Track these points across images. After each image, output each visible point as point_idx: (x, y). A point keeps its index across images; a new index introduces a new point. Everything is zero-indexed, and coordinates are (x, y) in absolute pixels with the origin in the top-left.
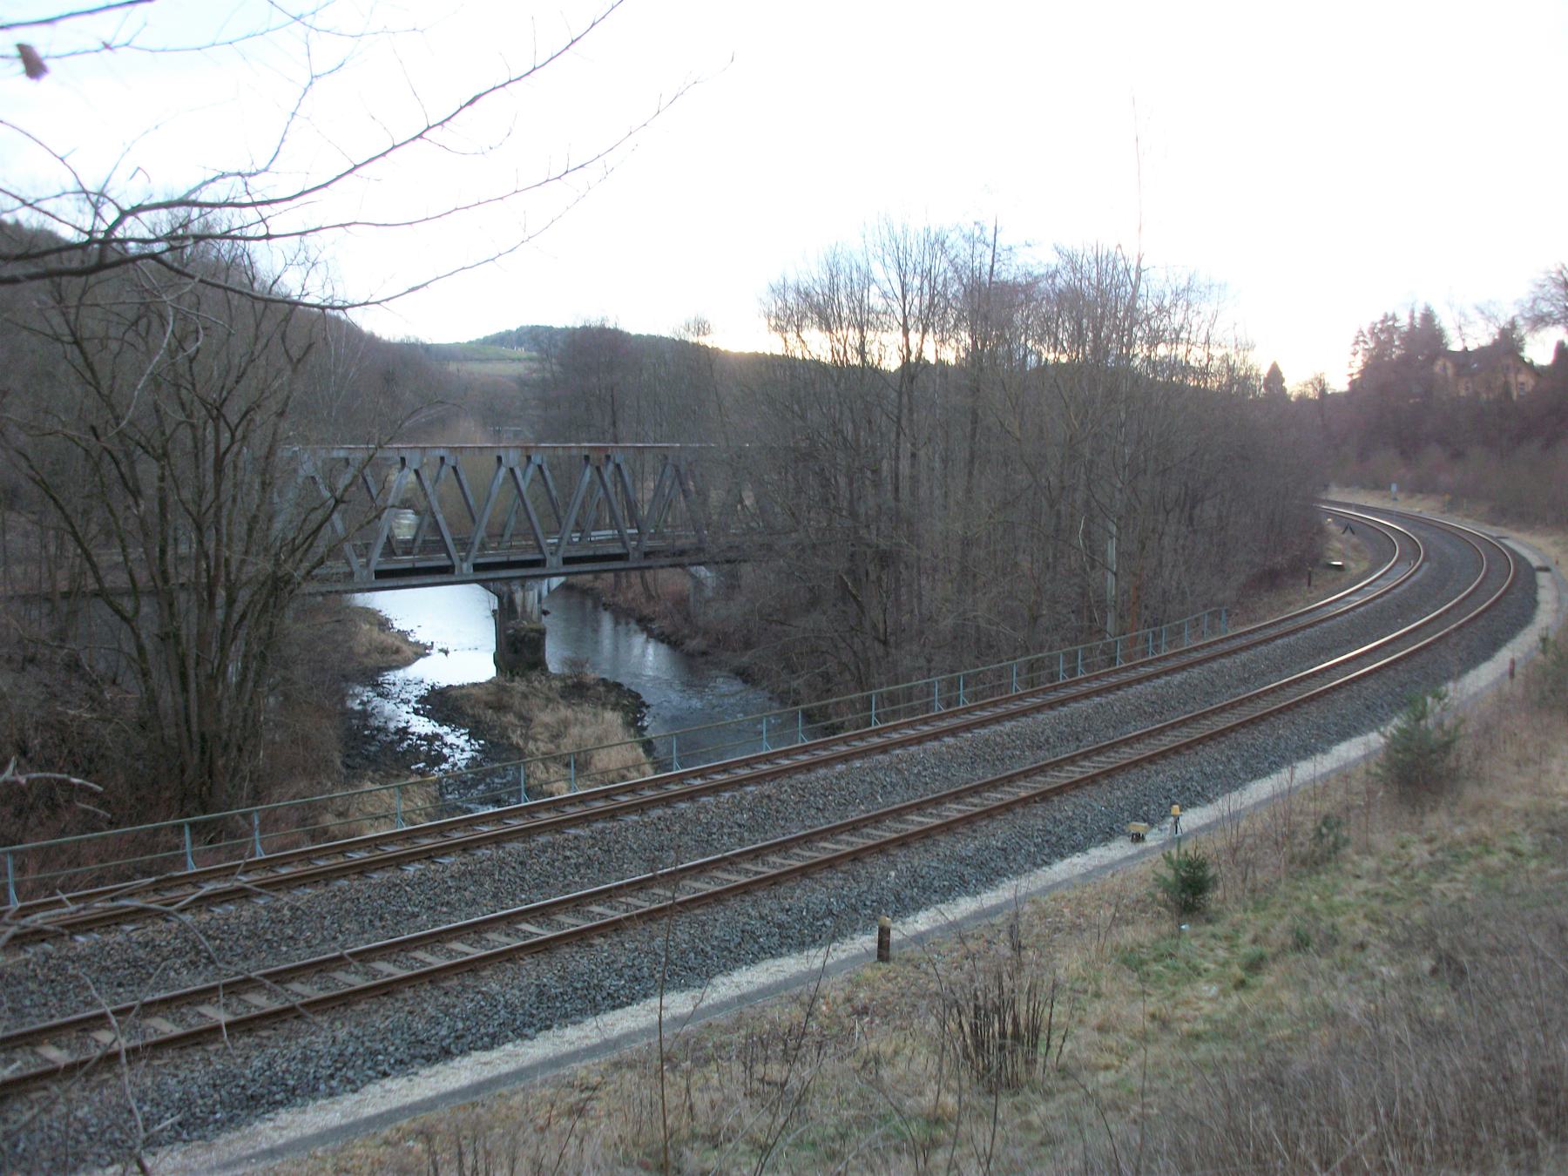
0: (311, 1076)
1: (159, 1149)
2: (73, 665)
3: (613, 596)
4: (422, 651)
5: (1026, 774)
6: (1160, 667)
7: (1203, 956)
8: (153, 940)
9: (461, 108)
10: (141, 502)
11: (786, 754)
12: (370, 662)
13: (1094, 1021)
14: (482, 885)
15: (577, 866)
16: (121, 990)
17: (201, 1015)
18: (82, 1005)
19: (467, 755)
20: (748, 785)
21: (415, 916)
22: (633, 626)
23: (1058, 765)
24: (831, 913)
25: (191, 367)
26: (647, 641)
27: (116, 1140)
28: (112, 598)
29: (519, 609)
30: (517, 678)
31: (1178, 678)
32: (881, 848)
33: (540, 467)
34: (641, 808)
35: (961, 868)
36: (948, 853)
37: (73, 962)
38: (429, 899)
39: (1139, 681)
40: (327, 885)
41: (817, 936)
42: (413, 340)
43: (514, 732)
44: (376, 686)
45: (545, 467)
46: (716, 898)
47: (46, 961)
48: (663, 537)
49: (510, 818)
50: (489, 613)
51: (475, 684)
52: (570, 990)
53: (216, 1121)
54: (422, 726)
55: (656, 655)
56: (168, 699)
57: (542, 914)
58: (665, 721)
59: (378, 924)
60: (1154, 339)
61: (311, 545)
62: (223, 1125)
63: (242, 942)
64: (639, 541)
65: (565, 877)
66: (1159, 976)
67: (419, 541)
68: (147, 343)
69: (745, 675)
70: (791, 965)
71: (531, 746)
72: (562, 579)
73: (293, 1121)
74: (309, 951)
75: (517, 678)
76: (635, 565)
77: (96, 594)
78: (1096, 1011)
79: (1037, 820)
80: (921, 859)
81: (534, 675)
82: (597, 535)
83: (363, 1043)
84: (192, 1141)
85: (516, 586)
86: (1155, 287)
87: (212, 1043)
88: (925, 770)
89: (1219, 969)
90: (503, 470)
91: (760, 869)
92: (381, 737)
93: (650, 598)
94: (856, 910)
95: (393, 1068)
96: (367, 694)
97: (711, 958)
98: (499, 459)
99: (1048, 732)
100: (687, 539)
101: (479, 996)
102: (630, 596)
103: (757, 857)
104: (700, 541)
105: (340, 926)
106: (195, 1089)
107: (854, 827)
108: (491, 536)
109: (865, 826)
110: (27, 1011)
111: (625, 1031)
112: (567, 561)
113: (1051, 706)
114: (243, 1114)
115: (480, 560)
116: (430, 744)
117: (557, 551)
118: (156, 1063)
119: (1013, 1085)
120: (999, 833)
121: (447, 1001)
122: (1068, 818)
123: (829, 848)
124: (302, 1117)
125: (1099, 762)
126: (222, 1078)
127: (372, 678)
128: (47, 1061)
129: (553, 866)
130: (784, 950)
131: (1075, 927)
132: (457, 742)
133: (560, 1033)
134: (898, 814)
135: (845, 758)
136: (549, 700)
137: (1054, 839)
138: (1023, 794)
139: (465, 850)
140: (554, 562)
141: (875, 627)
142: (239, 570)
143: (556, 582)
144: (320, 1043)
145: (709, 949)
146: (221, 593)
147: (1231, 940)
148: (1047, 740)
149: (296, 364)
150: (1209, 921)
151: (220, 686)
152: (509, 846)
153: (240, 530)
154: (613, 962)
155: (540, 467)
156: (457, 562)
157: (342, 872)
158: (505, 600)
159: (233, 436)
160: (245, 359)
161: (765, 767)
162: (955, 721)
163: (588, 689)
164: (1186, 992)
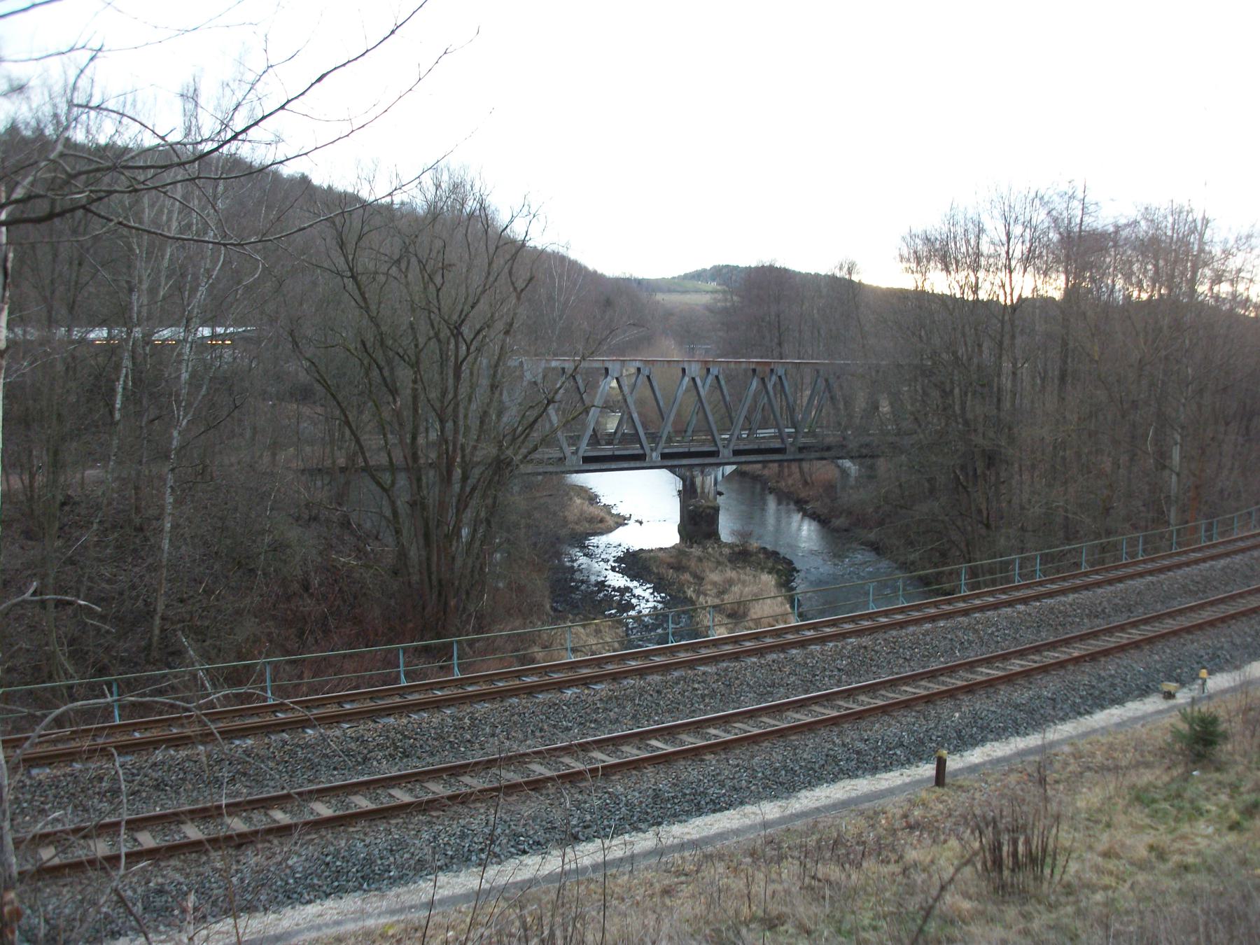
0: (466, 849)
1: (345, 895)
2: (345, 524)
3: (777, 482)
4: (621, 521)
5: (1082, 638)
6: (1208, 553)
7: (1207, 799)
8: (363, 736)
9: (312, 84)
10: (398, 399)
11: (886, 613)
12: (579, 529)
13: (1101, 847)
14: (624, 708)
15: (703, 696)
16: (336, 773)
17: (391, 796)
18: (306, 781)
19: (651, 604)
20: (850, 637)
21: (568, 729)
22: (792, 506)
23: (1109, 631)
24: (902, 745)
25: (438, 295)
26: (802, 518)
27: (314, 885)
28: (374, 473)
29: (699, 490)
30: (695, 545)
31: (1222, 562)
32: (951, 694)
33: (717, 377)
34: (760, 652)
35: (1015, 713)
36: (1005, 700)
37: (303, 749)
38: (581, 717)
39: (1188, 564)
40: (502, 701)
41: (888, 763)
42: (628, 276)
43: (689, 588)
44: (583, 547)
45: (721, 377)
46: (810, 727)
47: (283, 747)
48: (814, 435)
49: (655, 656)
50: (676, 493)
51: (661, 549)
52: (680, 795)
53: (390, 878)
54: (617, 580)
55: (809, 530)
56: (415, 553)
57: (669, 733)
58: (811, 583)
59: (538, 734)
60: (1218, 279)
61: (528, 434)
62: (395, 881)
63: (430, 742)
64: (795, 438)
65: (692, 705)
66: (1166, 813)
67: (619, 434)
68: (406, 277)
69: (877, 548)
70: (863, 785)
71: (701, 599)
72: (734, 467)
73: (448, 883)
74: (482, 752)
75: (695, 545)
76: (791, 457)
77: (364, 470)
78: (1104, 840)
79: (1084, 676)
80: (981, 704)
81: (709, 543)
82: (762, 433)
83: (509, 826)
84: (370, 891)
85: (697, 472)
86: (1217, 237)
87: (395, 818)
88: (998, 631)
89: (1220, 811)
90: (686, 379)
91: (850, 705)
92: (583, 587)
93: (806, 483)
94: (923, 743)
95: (531, 848)
96: (576, 552)
97: (799, 776)
98: (684, 370)
99: (1105, 604)
100: (832, 438)
101: (606, 796)
102: (790, 482)
103: (849, 696)
104: (844, 438)
105: (508, 734)
106: (376, 852)
107: (932, 675)
108: (677, 432)
109: (942, 675)
110: (266, 782)
111: (720, 831)
112: (737, 453)
113: (1110, 582)
114: (411, 874)
115: (666, 451)
116: (622, 595)
117: (728, 445)
118: (351, 829)
119: (1023, 895)
120: (1050, 686)
121: (580, 797)
122: (1111, 676)
123: (910, 691)
124: (455, 880)
125: (1144, 630)
126: (397, 845)
127: (580, 540)
128: (275, 821)
129: (683, 696)
130: (860, 772)
131: (1103, 769)
132: (643, 594)
133: (668, 829)
134: (970, 666)
135: (933, 619)
136: (719, 563)
137: (1097, 693)
138: (1076, 654)
139: (614, 679)
140: (726, 453)
141: (980, 511)
142: (472, 454)
143: (729, 469)
144: (476, 824)
145: (797, 768)
146: (458, 472)
147: (1234, 788)
148: (1103, 611)
149: (519, 294)
150: (1218, 770)
151: (454, 543)
152: (649, 678)
153: (474, 424)
154: (718, 774)
155: (717, 377)
156: (648, 451)
157: (514, 692)
158: (688, 483)
159: (468, 349)
160: (480, 289)
161: (866, 623)
162: (1030, 592)
163: (751, 556)
164: (1185, 828)
